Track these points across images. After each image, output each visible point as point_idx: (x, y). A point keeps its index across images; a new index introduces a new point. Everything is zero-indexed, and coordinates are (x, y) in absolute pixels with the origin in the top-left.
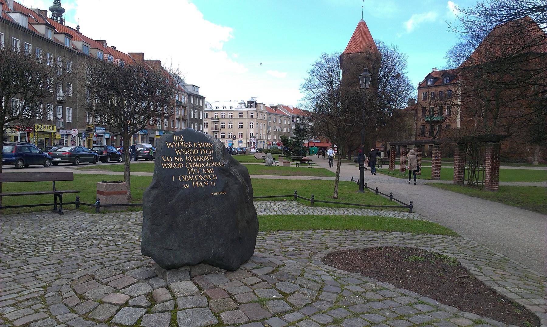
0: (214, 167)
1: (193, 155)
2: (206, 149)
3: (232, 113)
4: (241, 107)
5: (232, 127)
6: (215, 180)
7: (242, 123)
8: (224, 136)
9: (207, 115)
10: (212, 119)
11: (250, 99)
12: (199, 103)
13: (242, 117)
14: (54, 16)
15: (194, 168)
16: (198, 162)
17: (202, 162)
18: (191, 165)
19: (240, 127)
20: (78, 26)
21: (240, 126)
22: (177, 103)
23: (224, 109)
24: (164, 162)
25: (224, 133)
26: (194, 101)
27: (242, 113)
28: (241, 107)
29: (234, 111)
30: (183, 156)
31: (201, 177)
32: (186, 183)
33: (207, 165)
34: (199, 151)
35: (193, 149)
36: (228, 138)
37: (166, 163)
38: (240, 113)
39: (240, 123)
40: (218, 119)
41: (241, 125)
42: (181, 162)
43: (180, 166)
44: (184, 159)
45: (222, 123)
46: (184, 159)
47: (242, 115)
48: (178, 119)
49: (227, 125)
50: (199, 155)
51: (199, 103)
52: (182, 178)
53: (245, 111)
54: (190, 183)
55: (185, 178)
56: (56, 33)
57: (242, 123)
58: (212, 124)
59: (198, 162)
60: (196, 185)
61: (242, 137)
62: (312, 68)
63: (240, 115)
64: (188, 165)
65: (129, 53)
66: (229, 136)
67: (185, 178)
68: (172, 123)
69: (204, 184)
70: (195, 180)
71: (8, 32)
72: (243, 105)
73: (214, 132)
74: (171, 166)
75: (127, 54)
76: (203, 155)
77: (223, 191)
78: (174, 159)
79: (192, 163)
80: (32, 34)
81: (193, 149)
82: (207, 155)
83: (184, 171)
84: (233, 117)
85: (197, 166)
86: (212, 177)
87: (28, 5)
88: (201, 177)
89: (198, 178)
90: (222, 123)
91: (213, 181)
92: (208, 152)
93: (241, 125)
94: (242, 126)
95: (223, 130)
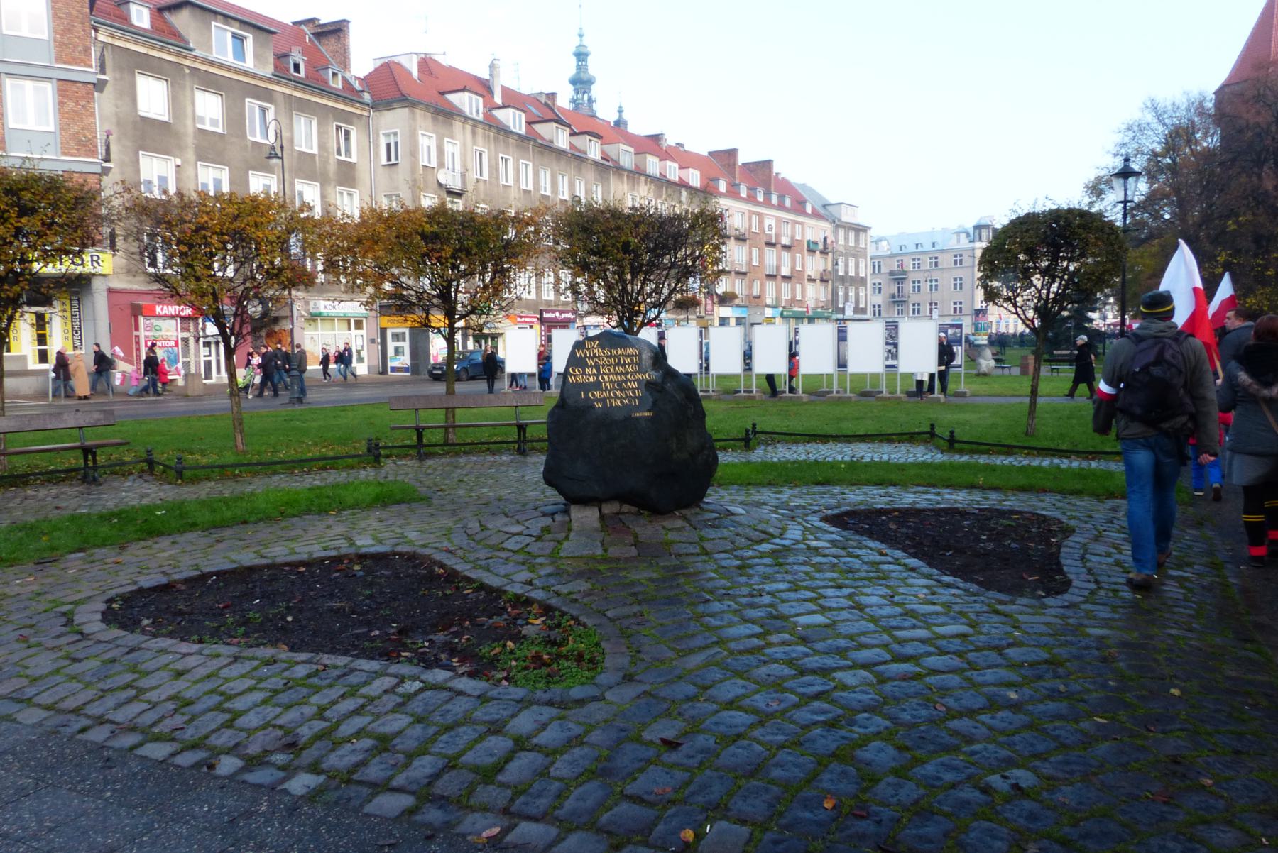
0: (638, 380)
1: (610, 365)
2: (628, 356)
3: (936, 258)
4: (958, 241)
5: (961, 288)
6: (639, 398)
7: (961, 279)
8: (919, 310)
9: (879, 266)
10: (891, 273)
11: (975, 222)
12: (857, 240)
13: (961, 264)
14: (578, 93)
15: (611, 381)
16: (617, 374)
17: (621, 374)
18: (606, 378)
19: (955, 288)
20: (620, 107)
21: (955, 285)
22: (808, 246)
23: (901, 249)
24: (571, 375)
25: (919, 304)
26: (846, 239)
27: (961, 255)
28: (958, 241)
29: (941, 251)
30: (597, 366)
31: (618, 393)
32: (598, 400)
33: (629, 377)
34: (619, 360)
35: (610, 357)
36: (952, 313)
37: (575, 376)
38: (956, 256)
39: (955, 279)
40: (905, 273)
41: (958, 282)
42: (594, 374)
43: (591, 379)
44: (598, 370)
45: (914, 282)
46: (598, 370)
47: (961, 260)
48: (811, 280)
49: (925, 287)
50: (618, 364)
51: (857, 240)
52: (593, 395)
53: (966, 250)
54: (603, 401)
55: (597, 394)
56: (573, 134)
57: (961, 279)
58: (892, 285)
59: (617, 374)
60: (611, 403)
61: (961, 311)
62: (1119, 138)
63: (956, 261)
64: (603, 378)
65: (710, 153)
66: (955, 309)
67: (597, 394)
68: (798, 287)
69: (622, 402)
70: (610, 397)
71: (492, 146)
72: (964, 236)
73: (894, 302)
74: (580, 380)
75: (706, 154)
76: (624, 365)
77: (649, 411)
78: (584, 371)
79: (608, 375)
80: (532, 143)
81: (610, 357)
82: (629, 364)
83: (597, 385)
84: (940, 267)
85: (614, 378)
86: (634, 393)
87: (526, 89)
88: (618, 393)
89: (615, 394)
90: (914, 282)
91: (634, 398)
92: (632, 360)
93: (958, 282)
94: (961, 284)
95: (915, 298)
